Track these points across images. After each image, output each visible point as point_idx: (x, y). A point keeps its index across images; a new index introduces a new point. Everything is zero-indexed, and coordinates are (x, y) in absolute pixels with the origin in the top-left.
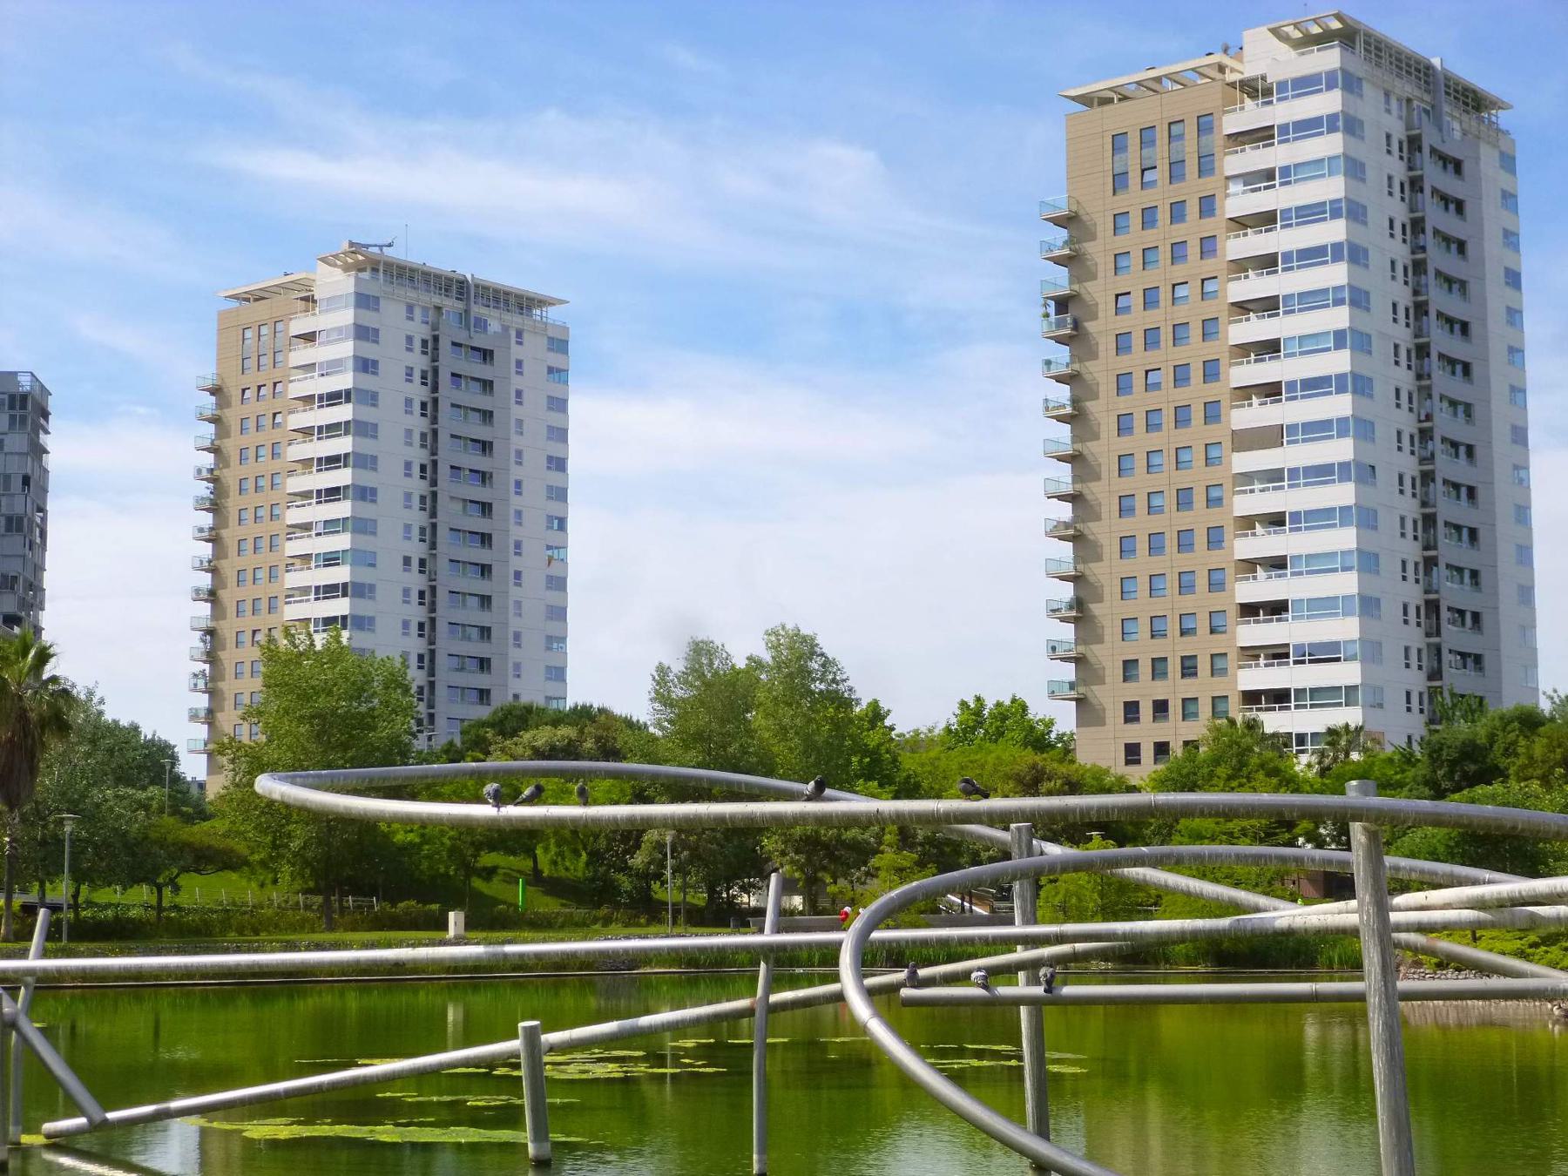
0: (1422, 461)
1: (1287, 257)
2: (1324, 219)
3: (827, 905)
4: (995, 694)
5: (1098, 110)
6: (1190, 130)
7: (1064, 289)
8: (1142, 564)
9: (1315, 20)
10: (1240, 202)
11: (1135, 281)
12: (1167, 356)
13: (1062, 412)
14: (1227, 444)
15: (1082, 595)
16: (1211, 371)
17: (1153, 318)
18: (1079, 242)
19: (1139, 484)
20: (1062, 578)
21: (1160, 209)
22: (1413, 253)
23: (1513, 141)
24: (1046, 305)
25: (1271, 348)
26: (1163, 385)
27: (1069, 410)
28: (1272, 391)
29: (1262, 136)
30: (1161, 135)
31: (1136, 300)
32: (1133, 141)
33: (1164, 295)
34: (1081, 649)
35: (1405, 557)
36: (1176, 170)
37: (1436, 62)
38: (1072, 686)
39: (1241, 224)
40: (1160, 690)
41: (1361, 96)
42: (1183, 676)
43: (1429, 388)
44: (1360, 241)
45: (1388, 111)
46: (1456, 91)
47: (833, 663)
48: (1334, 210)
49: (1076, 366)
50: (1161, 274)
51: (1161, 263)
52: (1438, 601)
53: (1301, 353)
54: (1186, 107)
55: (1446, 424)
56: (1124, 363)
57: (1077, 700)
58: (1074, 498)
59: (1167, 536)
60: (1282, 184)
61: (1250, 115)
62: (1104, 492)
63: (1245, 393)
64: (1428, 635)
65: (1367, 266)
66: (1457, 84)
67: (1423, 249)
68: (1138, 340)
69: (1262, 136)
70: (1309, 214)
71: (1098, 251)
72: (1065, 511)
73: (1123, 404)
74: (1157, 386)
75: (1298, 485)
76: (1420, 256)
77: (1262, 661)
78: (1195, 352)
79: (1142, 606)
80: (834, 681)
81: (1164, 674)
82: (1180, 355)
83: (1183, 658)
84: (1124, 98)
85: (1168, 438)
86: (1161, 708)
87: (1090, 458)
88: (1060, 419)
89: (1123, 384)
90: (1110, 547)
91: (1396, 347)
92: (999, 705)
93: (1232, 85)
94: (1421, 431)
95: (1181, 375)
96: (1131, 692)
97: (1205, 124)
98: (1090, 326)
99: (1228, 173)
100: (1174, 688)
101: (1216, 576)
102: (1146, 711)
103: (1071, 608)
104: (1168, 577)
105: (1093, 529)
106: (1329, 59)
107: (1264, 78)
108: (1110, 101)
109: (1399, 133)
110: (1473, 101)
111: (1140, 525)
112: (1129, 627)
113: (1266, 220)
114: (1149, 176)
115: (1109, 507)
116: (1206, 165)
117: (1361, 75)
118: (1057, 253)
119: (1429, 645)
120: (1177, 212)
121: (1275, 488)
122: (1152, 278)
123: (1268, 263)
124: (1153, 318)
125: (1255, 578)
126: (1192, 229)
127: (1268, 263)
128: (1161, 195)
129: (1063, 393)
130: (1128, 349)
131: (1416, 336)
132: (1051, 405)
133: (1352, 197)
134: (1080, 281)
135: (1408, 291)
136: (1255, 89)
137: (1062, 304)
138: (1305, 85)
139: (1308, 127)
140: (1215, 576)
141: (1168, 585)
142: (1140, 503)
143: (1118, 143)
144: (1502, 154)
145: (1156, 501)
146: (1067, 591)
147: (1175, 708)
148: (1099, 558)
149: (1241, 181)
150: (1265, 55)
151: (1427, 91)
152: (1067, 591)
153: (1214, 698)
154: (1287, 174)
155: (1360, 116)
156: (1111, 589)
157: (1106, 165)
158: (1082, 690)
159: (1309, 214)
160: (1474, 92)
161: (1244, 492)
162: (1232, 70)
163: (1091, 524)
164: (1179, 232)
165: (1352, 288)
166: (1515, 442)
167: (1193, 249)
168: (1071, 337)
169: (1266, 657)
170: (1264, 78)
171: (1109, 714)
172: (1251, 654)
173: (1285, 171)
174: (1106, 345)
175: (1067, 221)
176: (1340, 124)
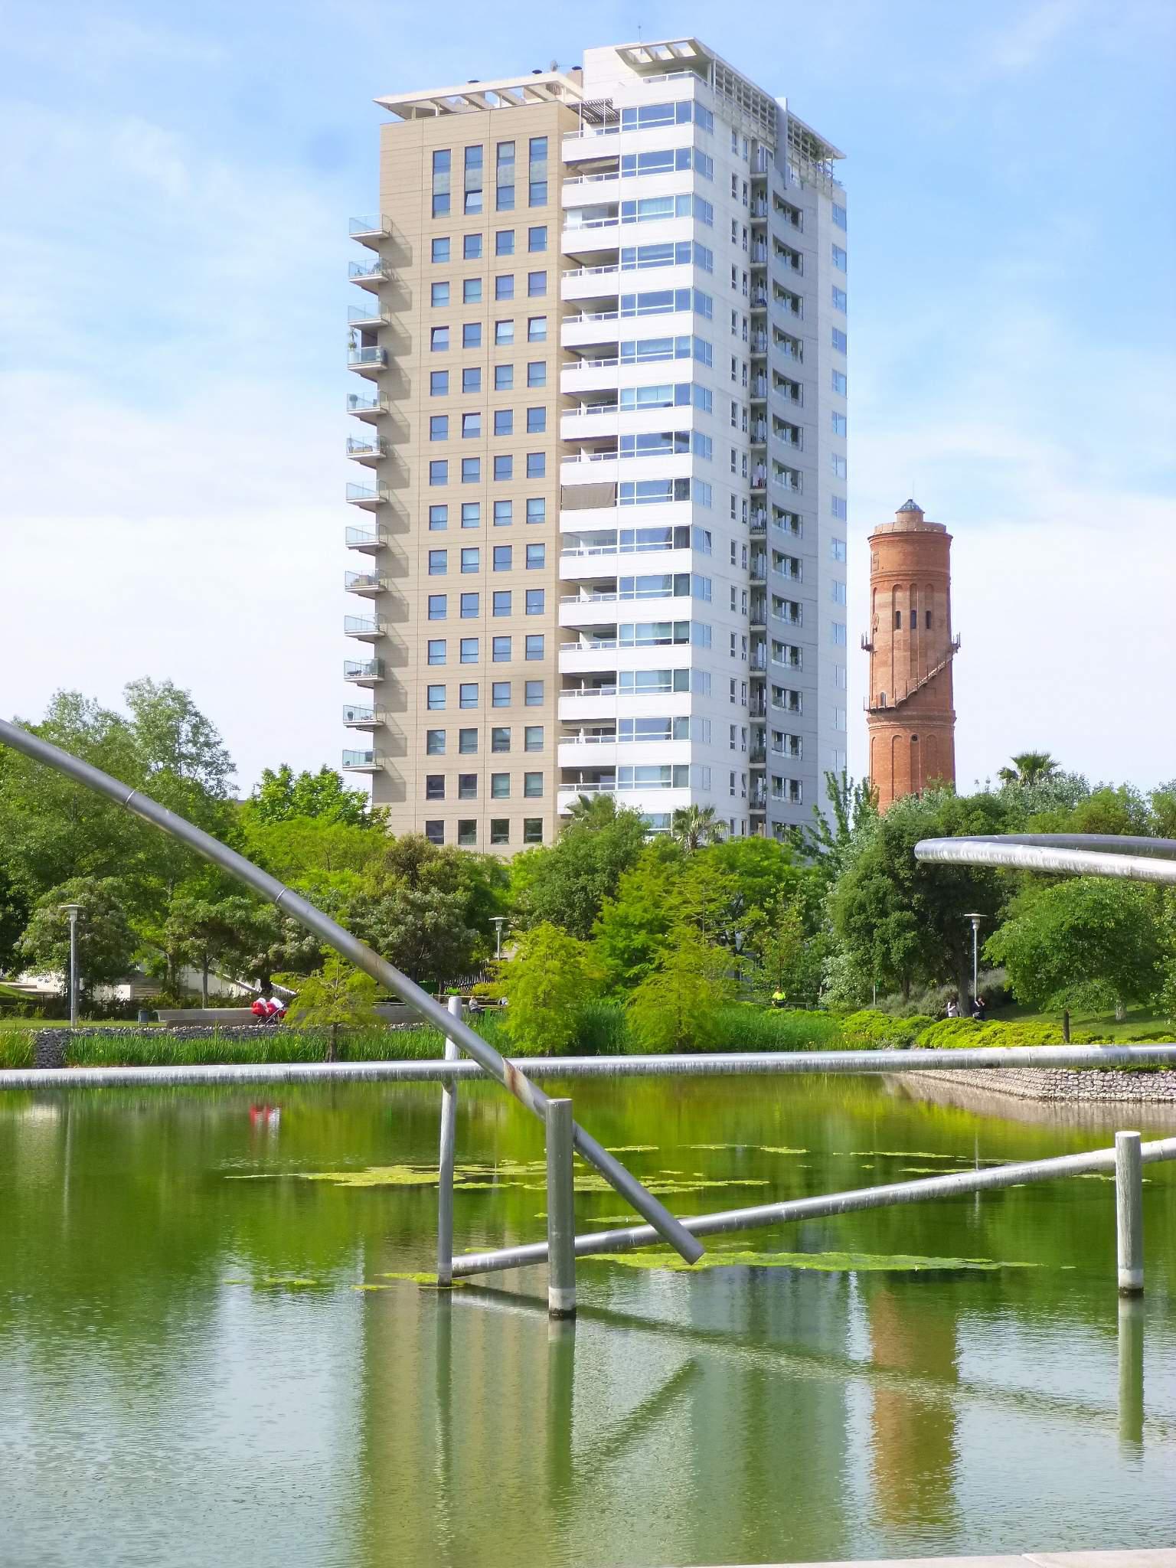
0: (754, 529)
1: (628, 301)
2: (670, 263)
3: (912, 993)
4: (306, 763)
5: (415, 123)
6: (522, 152)
7: (374, 319)
8: (452, 627)
9: (667, 45)
10: (580, 238)
11: (455, 314)
12: (487, 400)
13: (367, 454)
14: (551, 501)
15: (383, 657)
16: (536, 419)
17: (474, 357)
18: (392, 267)
19: (452, 538)
20: (361, 638)
21: (484, 237)
22: (752, 306)
23: (845, 194)
24: (353, 334)
25: (606, 399)
26: (483, 432)
27: (376, 453)
28: (605, 446)
29: (606, 168)
30: (489, 156)
31: (455, 335)
32: (457, 160)
33: (487, 333)
34: (382, 716)
35: (735, 631)
36: (504, 196)
37: (781, 101)
38: (369, 757)
39: (576, 261)
40: (468, 764)
41: (711, 131)
42: (494, 749)
43: (764, 452)
44: (707, 291)
45: (735, 151)
46: (797, 135)
47: (203, 722)
48: (680, 254)
49: (386, 405)
50: (484, 310)
51: (484, 297)
52: (764, 678)
53: (641, 407)
54: (521, 127)
55: (778, 491)
56: (439, 405)
57: (374, 772)
58: (379, 551)
59: (482, 597)
60: (625, 221)
61: (590, 144)
62: (412, 545)
63: (574, 447)
64: (752, 714)
65: (710, 317)
66: (798, 127)
67: (764, 303)
68: (455, 381)
69: (606, 168)
70: (654, 255)
71: (413, 278)
72: (368, 565)
73: (438, 450)
74: (476, 432)
75: (631, 549)
76: (760, 310)
77: (582, 736)
78: (518, 398)
79: (451, 672)
80: (207, 744)
81: (473, 747)
82: (503, 399)
83: (494, 730)
84: (445, 112)
85: (487, 490)
86: (468, 783)
87: (397, 507)
88: (364, 462)
89: (437, 427)
90: (417, 607)
91: (734, 405)
92: (306, 776)
93: (574, 108)
94: (754, 498)
95: (502, 422)
96: (435, 765)
97: (537, 149)
98: (402, 361)
99: (565, 204)
100: (484, 763)
101: (534, 643)
102: (451, 786)
103: (372, 672)
104: (481, 641)
105: (399, 586)
106: (683, 88)
107: (609, 103)
108: (430, 113)
109: (744, 177)
110: (812, 148)
111: (452, 583)
112: (436, 694)
113: (607, 259)
114: (473, 200)
115: (418, 564)
116: (537, 193)
117: (712, 109)
118: (366, 277)
119: (752, 725)
120: (504, 242)
121: (605, 551)
122: (472, 313)
123: (606, 306)
124: (474, 357)
125: (580, 647)
126: (520, 262)
127: (606, 306)
128: (487, 222)
129: (369, 434)
130: (444, 389)
131: (752, 396)
132: (355, 446)
133: (700, 241)
134: (392, 311)
135: (746, 347)
136: (601, 117)
137: (371, 335)
138: (655, 115)
139: (654, 161)
140: (533, 643)
141: (481, 650)
142: (453, 560)
143: (440, 160)
144: (835, 206)
145: (470, 558)
146: (367, 653)
147: (484, 785)
148: (404, 619)
149: (580, 213)
150: (609, 79)
151: (771, 132)
152: (367, 653)
153: (494, 775)
154: (631, 209)
155: (709, 154)
156: (417, 653)
157: (425, 184)
158: (380, 761)
159: (654, 255)
160: (814, 138)
161: (573, 554)
162: (569, 91)
163: (397, 580)
164: (505, 264)
165: (698, 341)
166: (835, 514)
167: (521, 285)
168: (380, 372)
169: (587, 733)
170: (609, 103)
171: (410, 789)
172: (571, 728)
173: (630, 207)
174: (419, 384)
175: (379, 243)
176: (691, 160)
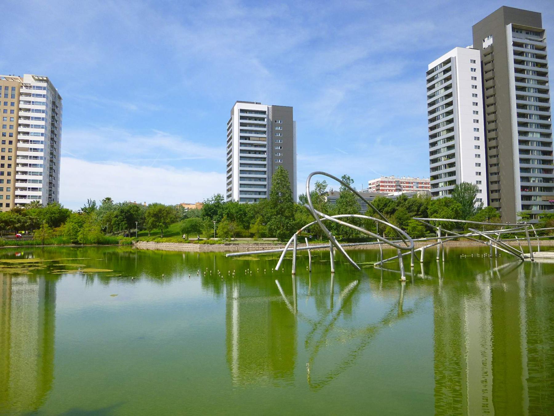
138: (39, 88)
